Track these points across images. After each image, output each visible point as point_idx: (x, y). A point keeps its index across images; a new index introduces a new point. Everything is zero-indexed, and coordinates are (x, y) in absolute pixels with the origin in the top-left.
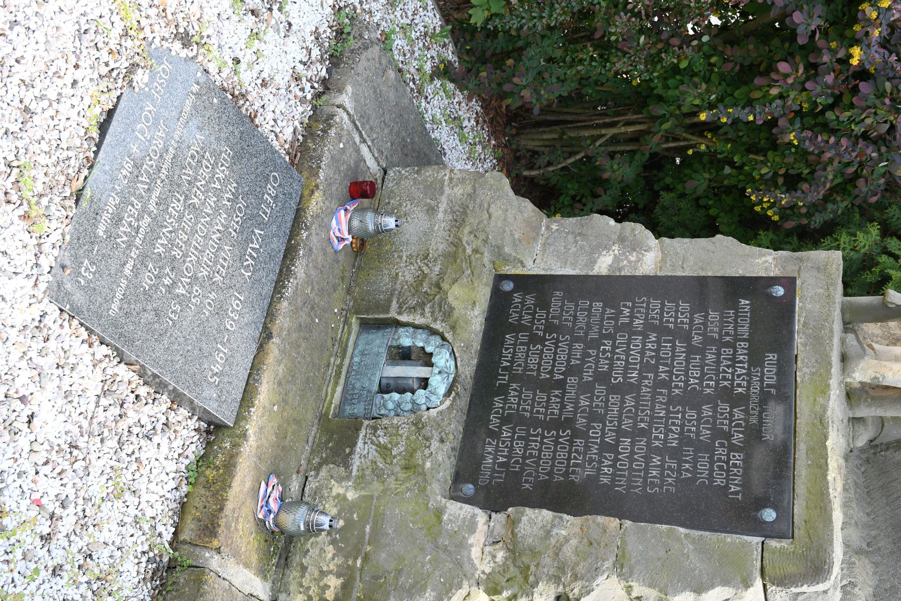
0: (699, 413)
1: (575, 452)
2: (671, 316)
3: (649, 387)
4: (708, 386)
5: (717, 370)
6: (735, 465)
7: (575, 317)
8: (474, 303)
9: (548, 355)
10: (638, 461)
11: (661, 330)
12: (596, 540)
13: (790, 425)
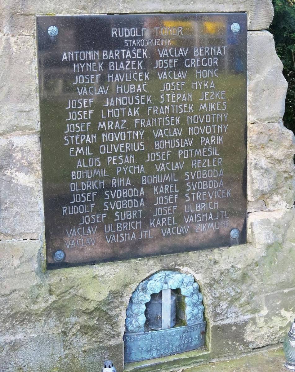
0: (164, 81)
1: (202, 165)
2: (82, 114)
3: (147, 121)
4: (143, 77)
5: (128, 72)
6: (203, 52)
7: (86, 192)
8: (94, 277)
9: (124, 204)
10: (205, 119)
11: (95, 120)
12: (269, 137)
13: (208, 15)
